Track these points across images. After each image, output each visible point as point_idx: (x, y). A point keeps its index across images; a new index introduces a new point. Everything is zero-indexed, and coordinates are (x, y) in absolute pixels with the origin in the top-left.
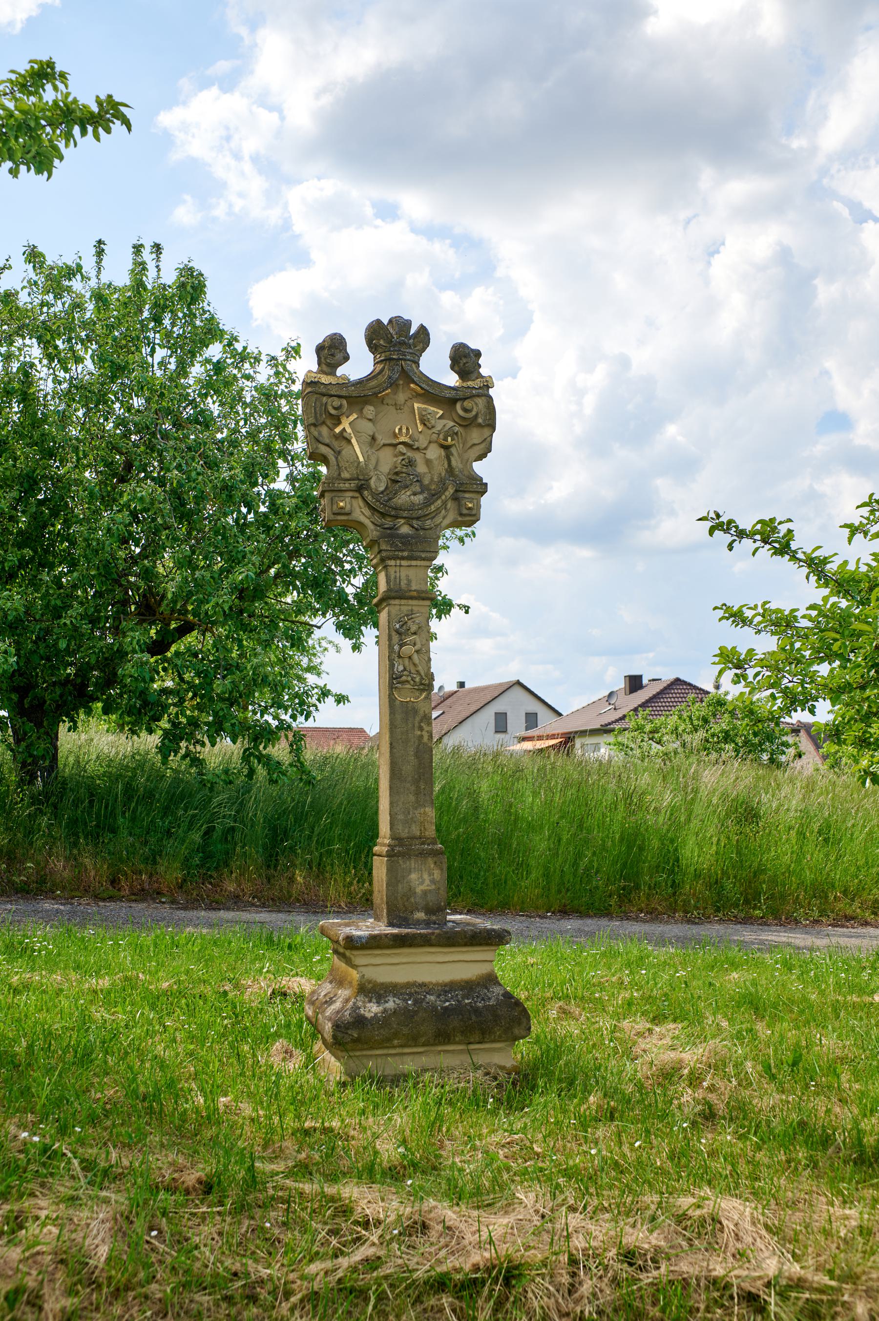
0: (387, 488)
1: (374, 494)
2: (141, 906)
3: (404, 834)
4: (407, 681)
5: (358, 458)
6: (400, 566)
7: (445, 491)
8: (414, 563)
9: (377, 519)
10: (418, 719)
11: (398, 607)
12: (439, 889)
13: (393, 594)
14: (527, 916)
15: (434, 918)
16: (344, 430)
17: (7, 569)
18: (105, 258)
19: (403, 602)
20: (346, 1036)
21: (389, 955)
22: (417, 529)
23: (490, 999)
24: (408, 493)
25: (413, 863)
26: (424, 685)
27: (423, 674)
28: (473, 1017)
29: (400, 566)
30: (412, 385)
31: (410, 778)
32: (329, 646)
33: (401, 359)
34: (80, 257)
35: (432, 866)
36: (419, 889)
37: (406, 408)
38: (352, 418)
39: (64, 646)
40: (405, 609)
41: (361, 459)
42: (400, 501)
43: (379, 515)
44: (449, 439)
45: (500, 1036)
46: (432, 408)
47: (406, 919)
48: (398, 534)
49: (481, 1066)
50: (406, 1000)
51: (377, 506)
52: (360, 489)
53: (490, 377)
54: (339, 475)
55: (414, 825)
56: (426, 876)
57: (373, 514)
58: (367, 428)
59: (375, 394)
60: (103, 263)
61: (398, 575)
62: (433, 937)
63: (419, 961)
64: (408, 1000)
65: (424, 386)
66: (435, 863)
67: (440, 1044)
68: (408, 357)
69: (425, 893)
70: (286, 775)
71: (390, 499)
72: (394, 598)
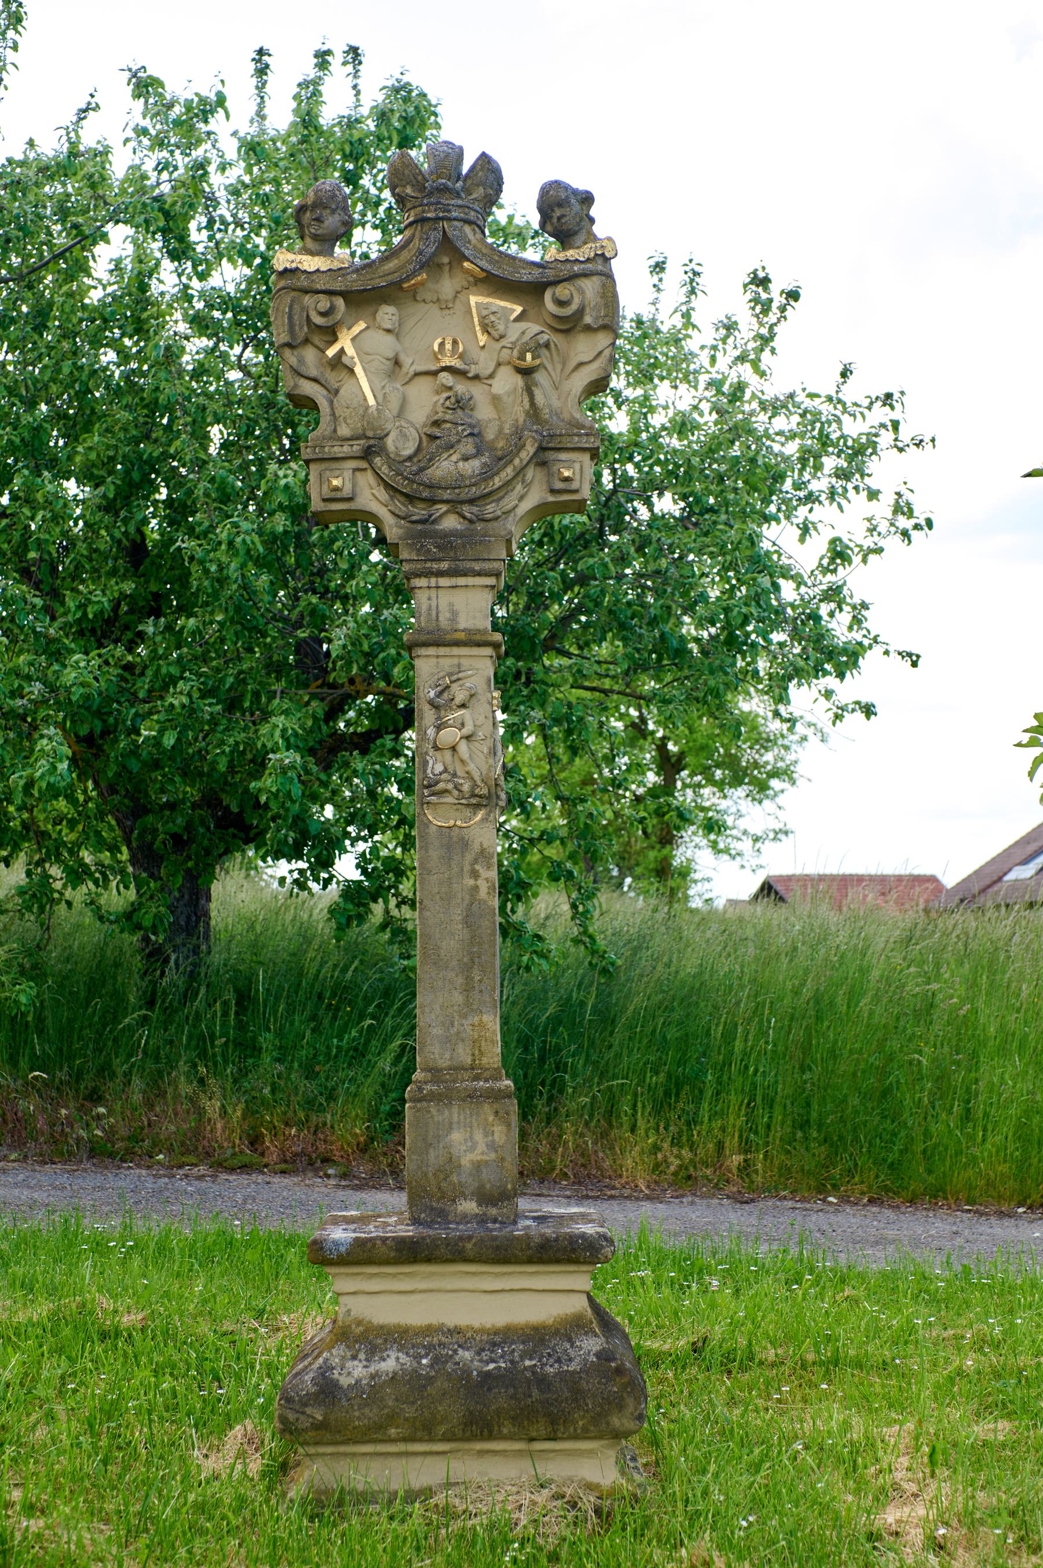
0: (419, 449)
1: (391, 462)
2: (287, 1181)
3: (443, 1062)
4: (446, 791)
5: (365, 399)
6: (438, 587)
7: (519, 451)
8: (461, 581)
9: (401, 507)
10: (469, 857)
11: (435, 660)
12: (503, 1159)
13: (423, 638)
14: (976, 1212)
15: (493, 1211)
16: (342, 351)
17: (91, 616)
18: (270, 77)
19: (442, 651)
20: (302, 1417)
21: (394, 1276)
22: (471, 521)
23: (570, 1360)
24: (454, 458)
25: (455, 1113)
26: (480, 796)
27: (477, 777)
28: (535, 1393)
29: (438, 587)
30: (466, 264)
31: (455, 963)
32: (809, 732)
33: (442, 219)
34: (222, 81)
35: (491, 1119)
36: (467, 1160)
37: (458, 305)
38: (356, 329)
39: (172, 742)
40: (447, 664)
41: (371, 401)
42: (439, 473)
43: (403, 499)
44: (529, 356)
45: (585, 1429)
46: (503, 304)
47: (442, 1213)
48: (436, 532)
49: (551, 1481)
50: (418, 1357)
51: (400, 483)
52: (367, 454)
53: (610, 239)
54: (335, 431)
55: (460, 1045)
56: (479, 1136)
57: (392, 498)
58: (384, 344)
59: (397, 285)
60: (268, 88)
61: (434, 604)
62: (469, 1246)
63: (449, 1287)
64: (422, 1357)
65: (481, 263)
66: (497, 1113)
67: (482, 1438)
68: (454, 214)
69: (478, 1166)
70: (546, 958)
71: (421, 470)
72: (425, 644)
